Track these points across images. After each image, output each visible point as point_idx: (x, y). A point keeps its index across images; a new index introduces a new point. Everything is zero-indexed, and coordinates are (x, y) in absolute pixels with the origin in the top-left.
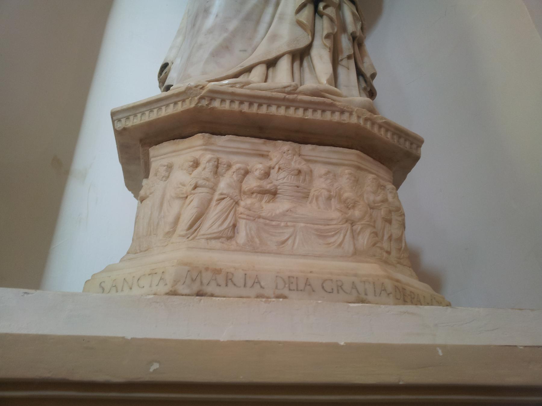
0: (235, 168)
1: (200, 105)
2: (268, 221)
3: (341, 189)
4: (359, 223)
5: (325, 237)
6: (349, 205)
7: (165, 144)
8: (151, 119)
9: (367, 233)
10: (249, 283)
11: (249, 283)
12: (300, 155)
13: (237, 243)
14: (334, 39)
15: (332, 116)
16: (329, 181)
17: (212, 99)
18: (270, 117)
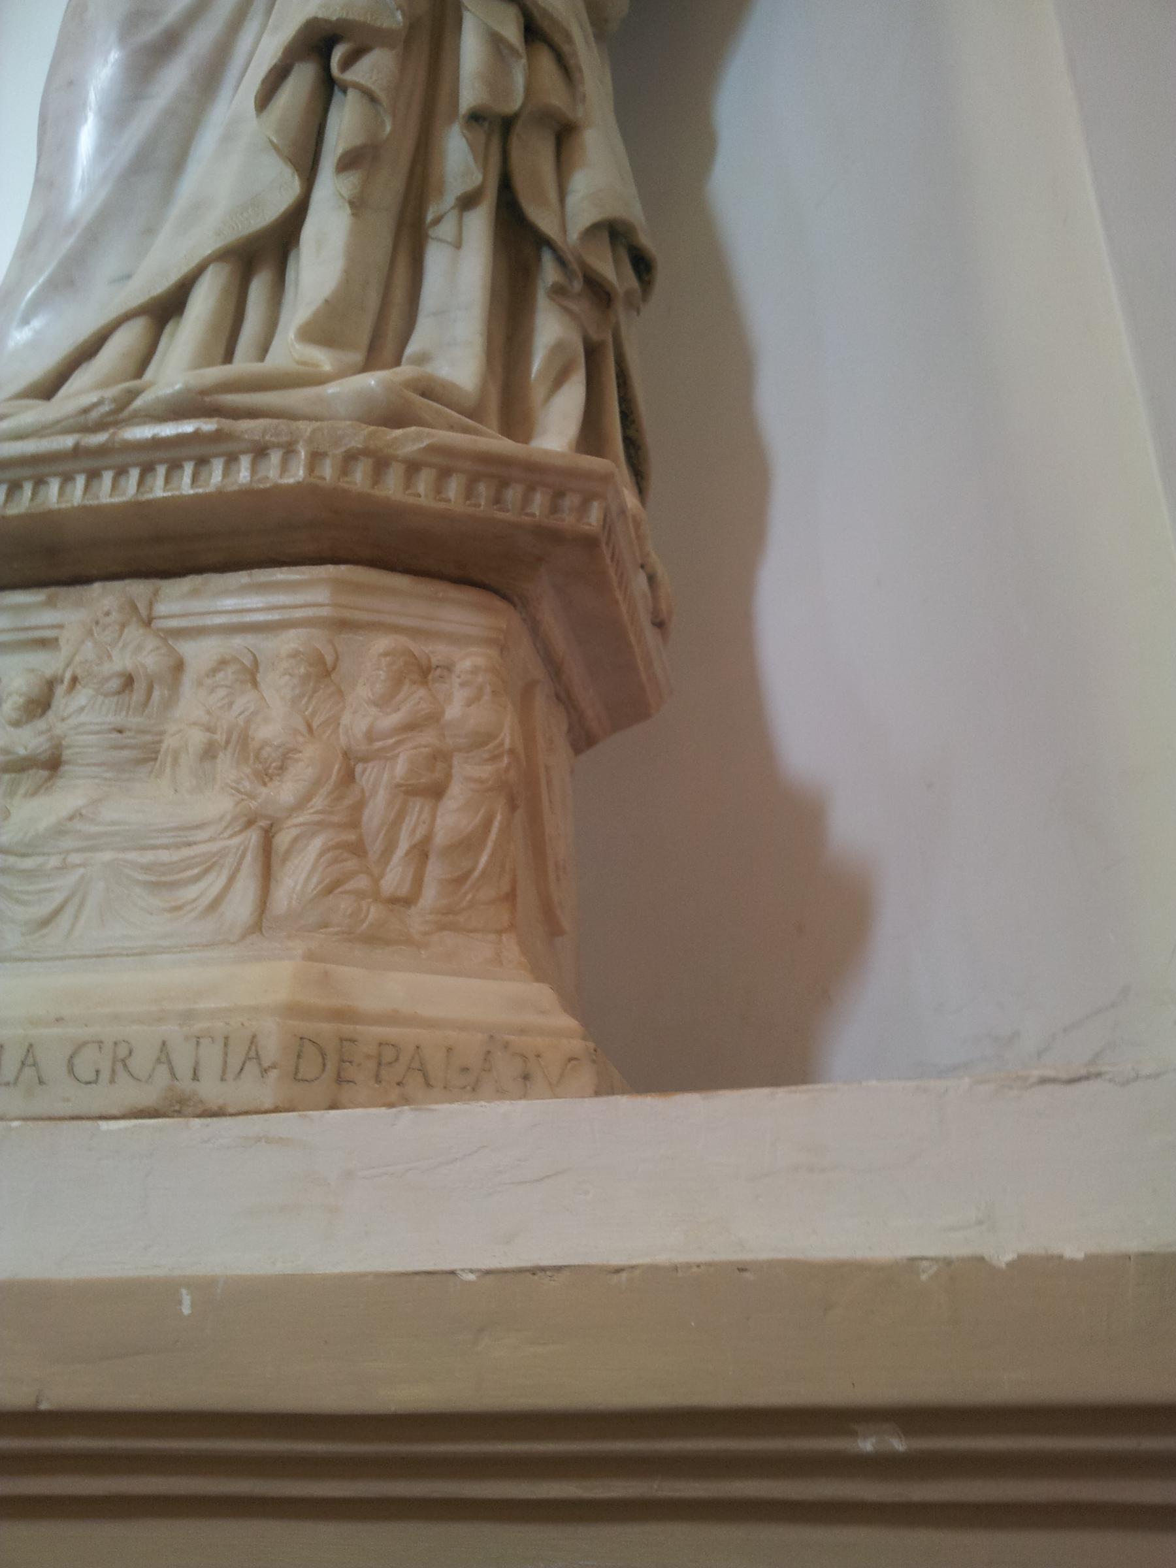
4: (290, 822)
5: (173, 885)
12: (148, 622)
16: (221, 692)
18: (49, 519)
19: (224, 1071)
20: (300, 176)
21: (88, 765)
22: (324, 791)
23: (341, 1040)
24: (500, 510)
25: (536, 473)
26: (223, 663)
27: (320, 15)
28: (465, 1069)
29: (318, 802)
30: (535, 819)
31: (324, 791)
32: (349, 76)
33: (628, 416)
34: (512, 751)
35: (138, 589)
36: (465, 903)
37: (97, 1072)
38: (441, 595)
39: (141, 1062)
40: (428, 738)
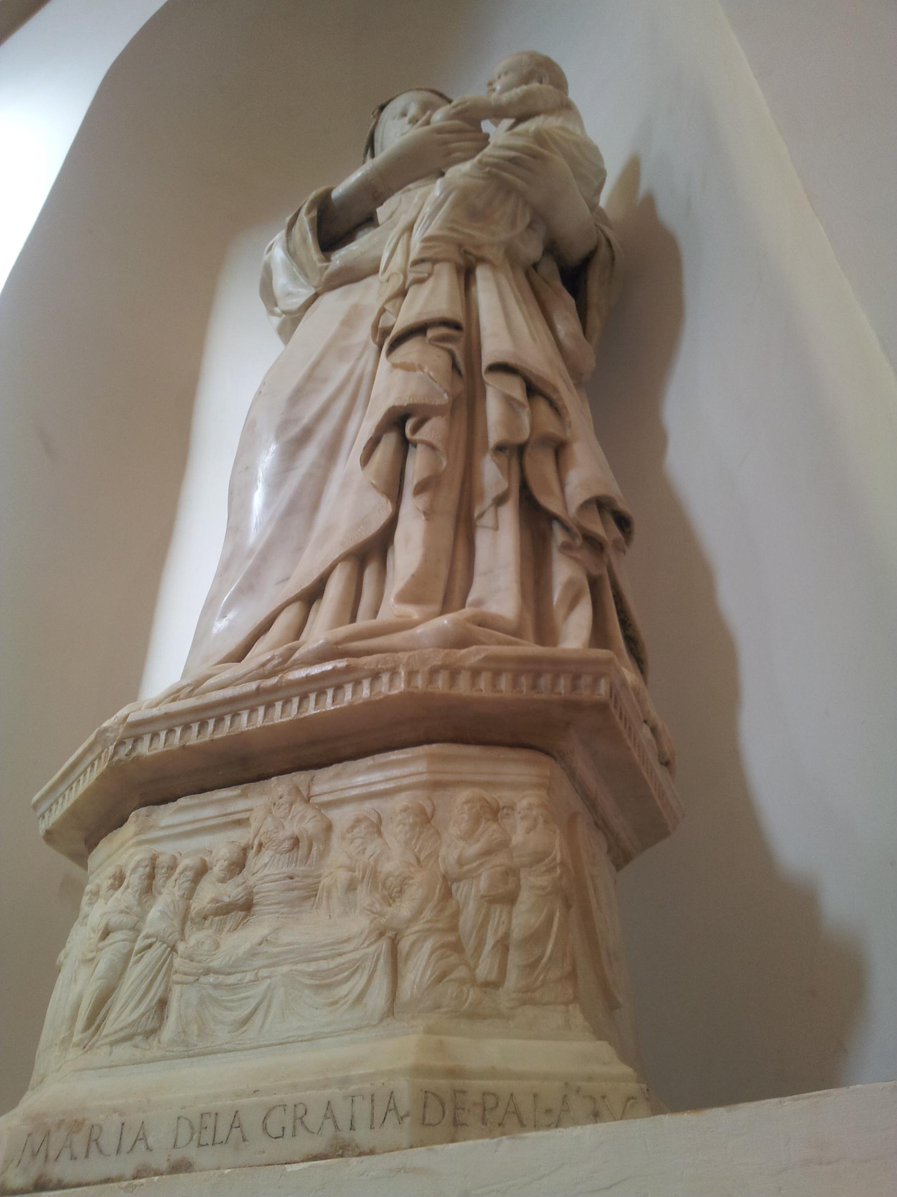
1: (116, 758)
4: (409, 931)
5: (329, 986)
10: (127, 1143)
11: (127, 1143)
12: (308, 800)
16: (358, 842)
17: (137, 739)
18: (241, 738)
19: (372, 1123)
20: (391, 501)
21: (271, 904)
22: (430, 906)
23: (455, 1092)
24: (538, 693)
25: (560, 666)
26: (358, 821)
27: (396, 404)
28: (549, 1111)
29: (427, 914)
30: (587, 917)
31: (430, 906)
32: (417, 437)
33: (625, 622)
34: (562, 864)
35: (300, 778)
36: (538, 983)
37: (283, 1128)
38: (502, 756)
39: (313, 1119)
40: (500, 860)
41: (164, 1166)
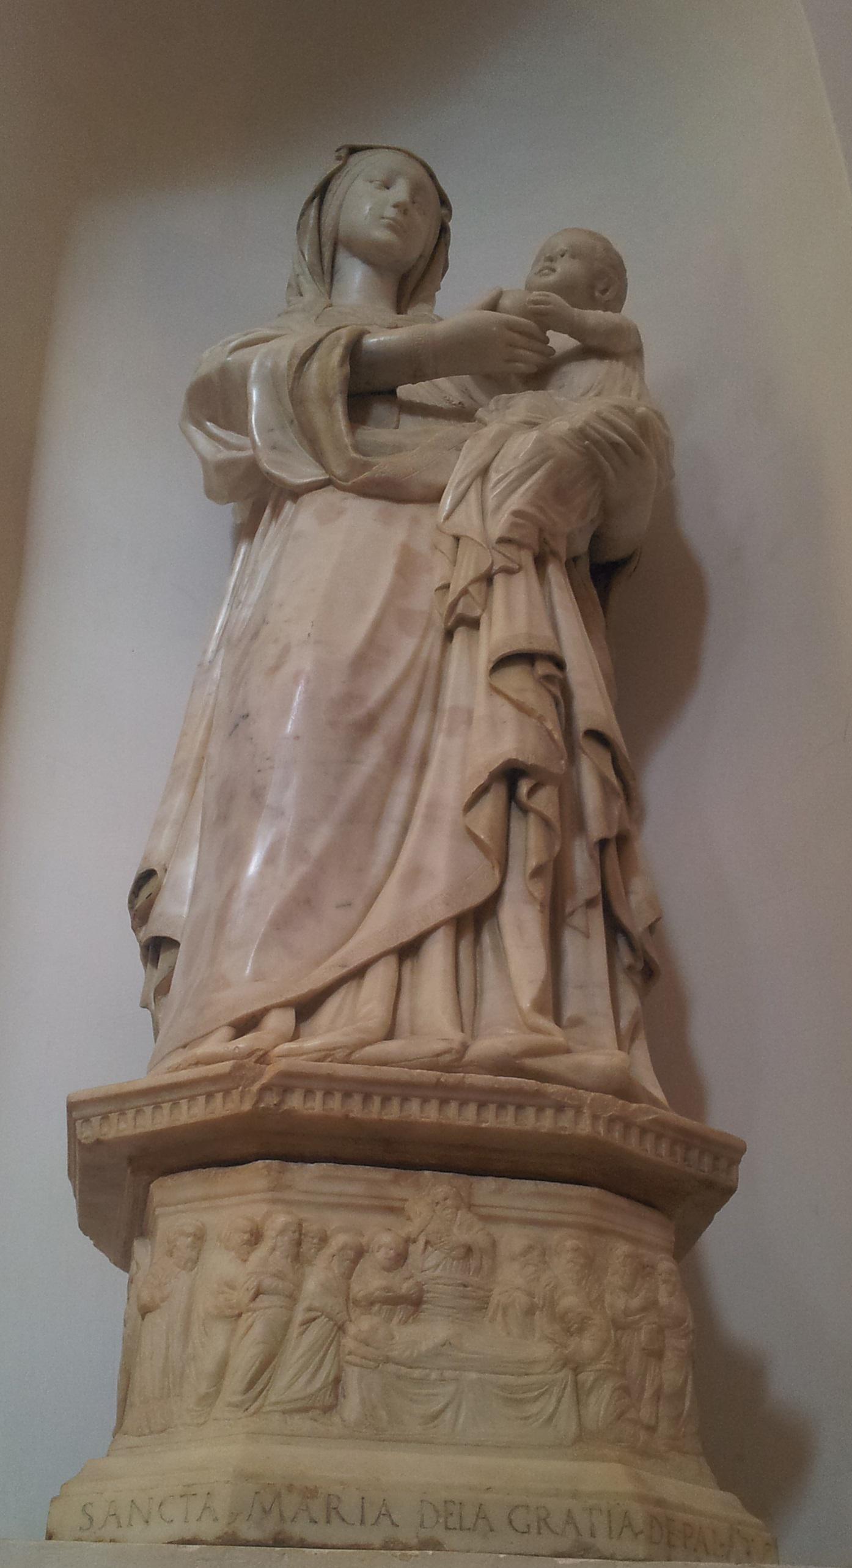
0: (338, 1241)
2: (404, 1370)
3: (555, 1287)
5: (521, 1401)
6: (571, 1326)
7: (187, 1176)
8: (158, 1127)
9: (606, 1390)
11: (370, 1517)
12: (470, 1207)
13: (343, 1421)
14: (555, 877)
15: (538, 1119)
16: (531, 1269)
17: (286, 1090)
28: (722, 1545)
35: (461, 1180)
41: (414, 1542)
